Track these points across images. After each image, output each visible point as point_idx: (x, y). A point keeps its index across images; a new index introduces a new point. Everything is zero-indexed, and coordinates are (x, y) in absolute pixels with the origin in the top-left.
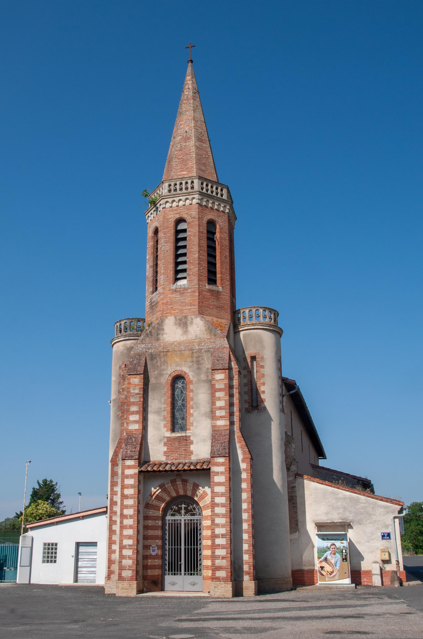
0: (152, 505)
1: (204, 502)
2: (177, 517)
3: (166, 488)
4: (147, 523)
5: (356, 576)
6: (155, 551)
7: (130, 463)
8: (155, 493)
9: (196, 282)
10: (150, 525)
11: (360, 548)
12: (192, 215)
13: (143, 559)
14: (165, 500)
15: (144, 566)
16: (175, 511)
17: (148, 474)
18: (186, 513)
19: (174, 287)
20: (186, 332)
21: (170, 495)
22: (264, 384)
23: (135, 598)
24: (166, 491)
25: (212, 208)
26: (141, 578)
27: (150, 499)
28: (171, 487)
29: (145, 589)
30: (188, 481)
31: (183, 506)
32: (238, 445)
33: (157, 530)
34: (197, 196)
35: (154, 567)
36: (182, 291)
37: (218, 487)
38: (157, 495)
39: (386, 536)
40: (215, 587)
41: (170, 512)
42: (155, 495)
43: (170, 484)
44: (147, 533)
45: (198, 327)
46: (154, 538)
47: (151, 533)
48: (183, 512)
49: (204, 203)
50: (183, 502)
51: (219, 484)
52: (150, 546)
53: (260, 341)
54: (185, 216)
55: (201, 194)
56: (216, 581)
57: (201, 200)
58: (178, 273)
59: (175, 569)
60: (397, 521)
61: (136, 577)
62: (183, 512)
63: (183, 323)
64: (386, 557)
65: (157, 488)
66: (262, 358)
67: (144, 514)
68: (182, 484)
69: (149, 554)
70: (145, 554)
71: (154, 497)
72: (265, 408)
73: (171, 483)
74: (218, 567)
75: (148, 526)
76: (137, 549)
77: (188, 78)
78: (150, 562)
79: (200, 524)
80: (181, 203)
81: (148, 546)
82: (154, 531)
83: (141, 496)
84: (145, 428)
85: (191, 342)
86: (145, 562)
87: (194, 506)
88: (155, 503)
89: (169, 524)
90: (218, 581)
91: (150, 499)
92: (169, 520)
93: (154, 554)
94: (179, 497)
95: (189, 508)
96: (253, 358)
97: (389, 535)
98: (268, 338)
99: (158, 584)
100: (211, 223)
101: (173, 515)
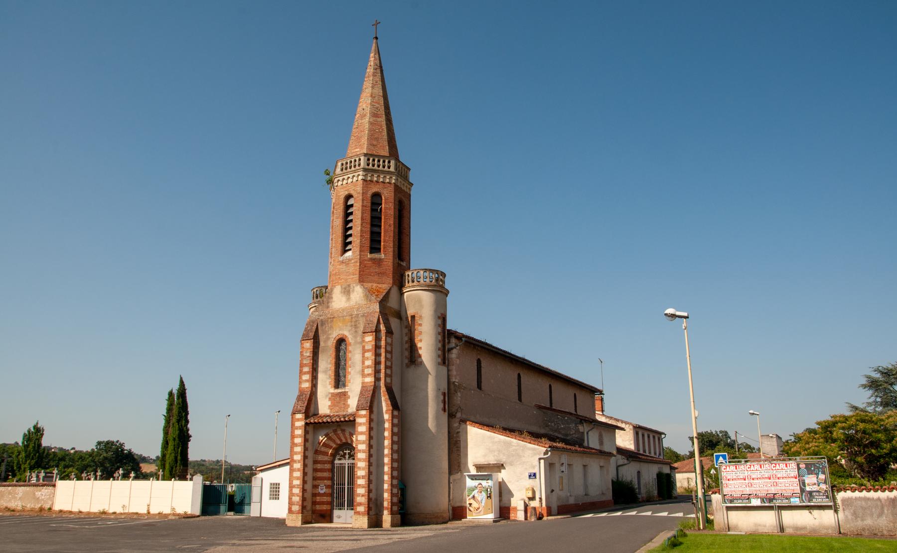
5: (504, 512)
7: (299, 416)
9: (358, 253)
11: (511, 487)
12: (357, 190)
17: (314, 424)
19: (341, 259)
20: (349, 299)
22: (421, 341)
23: (300, 528)
25: (377, 182)
32: (383, 399)
34: (361, 173)
36: (346, 263)
39: (533, 476)
41: (338, 457)
45: (358, 293)
48: (347, 456)
49: (369, 178)
51: (362, 433)
53: (419, 301)
54: (352, 192)
55: (365, 170)
57: (365, 176)
58: (345, 246)
59: (341, 506)
60: (542, 461)
62: (347, 456)
63: (347, 291)
64: (530, 495)
66: (421, 316)
72: (422, 363)
77: (372, 55)
80: (350, 180)
84: (314, 386)
85: (352, 308)
88: (323, 449)
93: (322, 492)
96: (413, 317)
97: (535, 475)
98: (427, 298)
99: (327, 517)
100: (377, 196)
101: (340, 459)
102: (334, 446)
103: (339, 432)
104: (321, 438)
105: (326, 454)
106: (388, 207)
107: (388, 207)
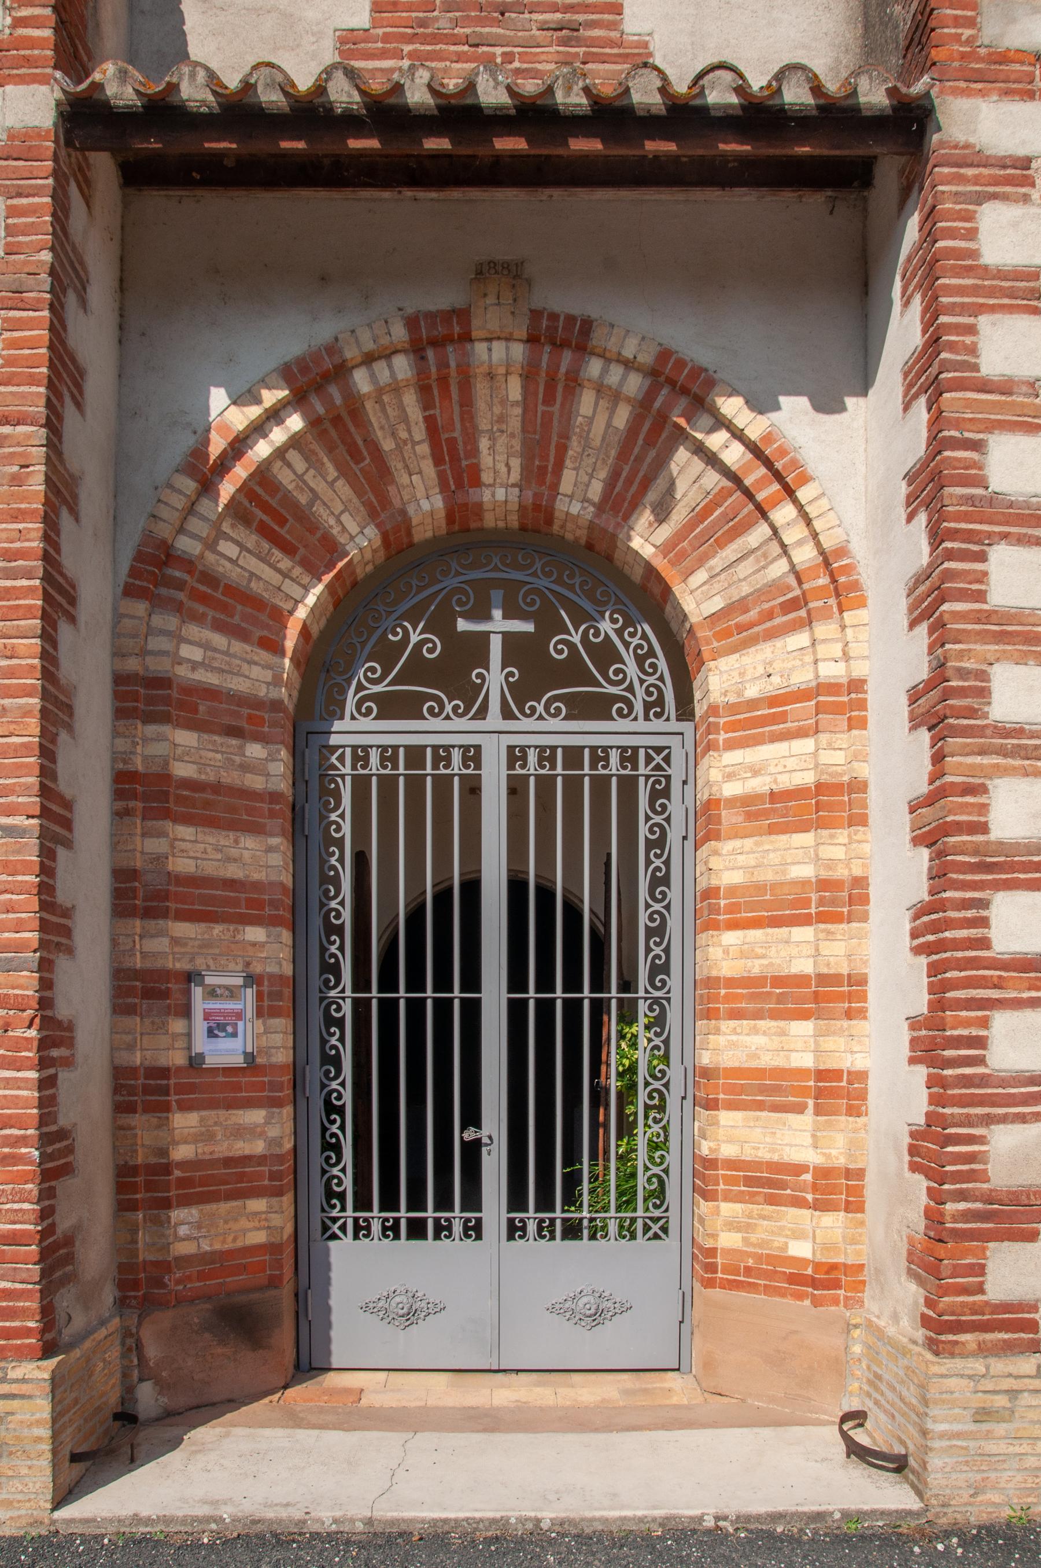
0: (210, 579)
1: (744, 569)
2: (439, 729)
3: (355, 407)
4: (158, 749)
6: (230, 1030)
8: (239, 446)
10: (182, 770)
13: (122, 1108)
14: (332, 549)
15: (126, 1178)
16: (418, 670)
18: (522, 695)
21: (384, 501)
24: (355, 454)
26: (109, 1295)
27: (191, 510)
28: (410, 399)
29: (148, 1398)
30: (598, 338)
31: (499, 625)
33: (255, 829)
35: (224, 1181)
37: (1022, 323)
38: (262, 474)
40: (983, 1415)
41: (368, 679)
42: (240, 472)
43: (402, 366)
44: (155, 845)
46: (221, 902)
47: (193, 850)
48: (495, 678)
50: (497, 595)
52: (190, 977)
56: (983, 1350)
61: (47, 1312)
62: (495, 678)
65: (271, 397)
67: (118, 653)
68: (528, 377)
69: (179, 1059)
70: (137, 1059)
71: (227, 489)
73: (417, 349)
74: (1015, 1197)
75: (166, 777)
76: (45, 1004)
78: (189, 1135)
79: (655, 795)
81: (166, 975)
82: (225, 839)
83: (88, 434)
86: (143, 1129)
87: (606, 626)
89: (361, 785)
90: (1008, 1349)
91: (191, 510)
92: (360, 755)
93: (225, 1052)
94: (466, 534)
95: (556, 650)
101: (391, 707)
102: (424, 502)
103: (498, 355)
104: (225, 413)
105: (250, 616)
106: (84, 186)
107: (84, 186)
